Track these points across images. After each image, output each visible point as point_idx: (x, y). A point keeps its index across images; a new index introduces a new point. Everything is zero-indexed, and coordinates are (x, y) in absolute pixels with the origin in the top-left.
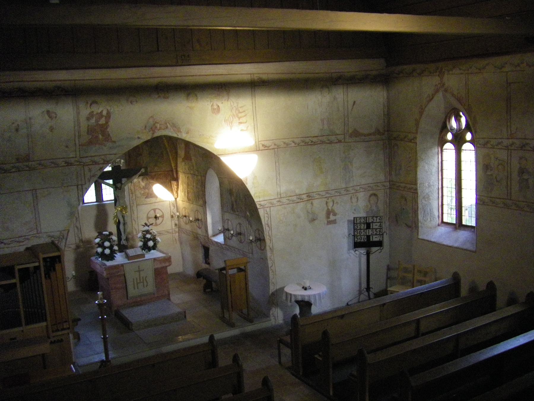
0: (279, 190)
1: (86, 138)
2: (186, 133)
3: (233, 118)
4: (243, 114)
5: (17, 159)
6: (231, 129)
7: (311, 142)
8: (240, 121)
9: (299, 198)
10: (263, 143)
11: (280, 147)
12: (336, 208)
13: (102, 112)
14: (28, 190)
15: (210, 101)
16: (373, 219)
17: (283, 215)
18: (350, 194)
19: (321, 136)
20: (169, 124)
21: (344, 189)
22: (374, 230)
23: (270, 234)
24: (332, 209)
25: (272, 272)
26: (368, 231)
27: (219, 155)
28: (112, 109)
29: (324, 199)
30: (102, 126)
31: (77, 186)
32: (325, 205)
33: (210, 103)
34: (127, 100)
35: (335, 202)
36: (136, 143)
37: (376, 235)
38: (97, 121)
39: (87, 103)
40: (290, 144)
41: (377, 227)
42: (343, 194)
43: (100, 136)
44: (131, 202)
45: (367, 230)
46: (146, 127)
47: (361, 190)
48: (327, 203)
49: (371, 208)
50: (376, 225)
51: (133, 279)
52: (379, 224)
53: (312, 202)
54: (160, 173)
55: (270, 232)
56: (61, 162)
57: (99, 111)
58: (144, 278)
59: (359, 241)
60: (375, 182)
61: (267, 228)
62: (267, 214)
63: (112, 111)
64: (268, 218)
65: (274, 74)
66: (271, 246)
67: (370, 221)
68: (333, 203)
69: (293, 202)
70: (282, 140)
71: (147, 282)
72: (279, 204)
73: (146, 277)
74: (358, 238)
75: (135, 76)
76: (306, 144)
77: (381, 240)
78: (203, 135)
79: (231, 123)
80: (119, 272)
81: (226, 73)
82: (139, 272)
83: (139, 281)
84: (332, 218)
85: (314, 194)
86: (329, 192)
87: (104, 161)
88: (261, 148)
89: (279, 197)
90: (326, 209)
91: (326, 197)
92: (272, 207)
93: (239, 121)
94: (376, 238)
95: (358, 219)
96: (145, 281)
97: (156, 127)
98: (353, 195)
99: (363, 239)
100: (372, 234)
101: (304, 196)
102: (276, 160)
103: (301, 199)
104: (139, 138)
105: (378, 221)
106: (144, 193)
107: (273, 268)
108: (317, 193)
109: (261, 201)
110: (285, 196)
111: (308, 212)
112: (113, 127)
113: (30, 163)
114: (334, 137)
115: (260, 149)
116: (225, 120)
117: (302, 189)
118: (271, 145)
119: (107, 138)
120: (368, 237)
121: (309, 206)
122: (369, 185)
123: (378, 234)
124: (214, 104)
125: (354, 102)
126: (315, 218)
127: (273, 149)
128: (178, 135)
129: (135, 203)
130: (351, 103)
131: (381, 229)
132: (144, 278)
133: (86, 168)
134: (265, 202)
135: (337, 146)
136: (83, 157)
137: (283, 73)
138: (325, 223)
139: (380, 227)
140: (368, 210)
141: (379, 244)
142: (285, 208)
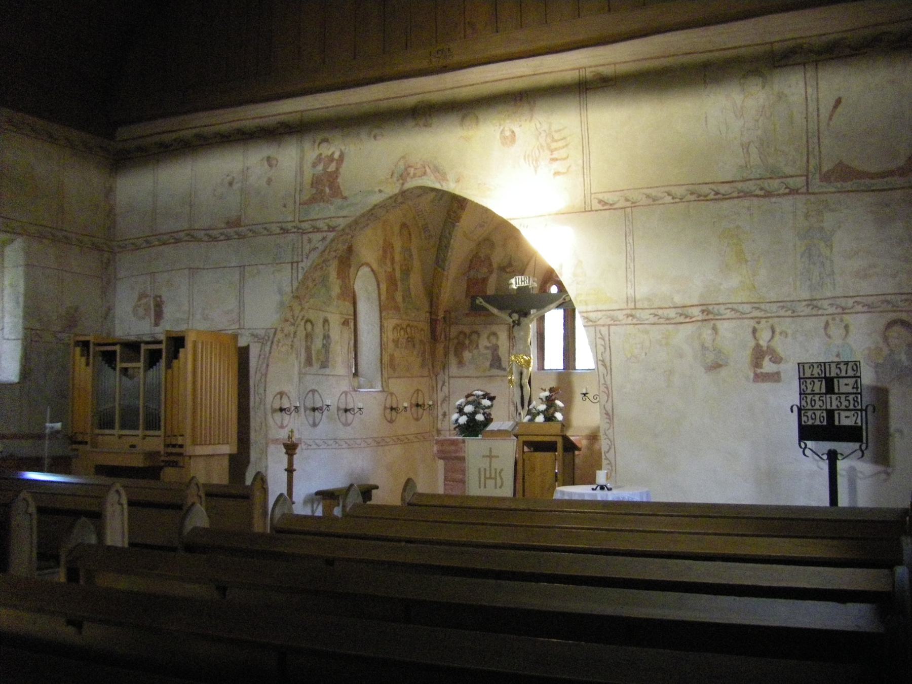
1: (306, 196)
2: (456, 182)
3: (539, 152)
4: (560, 144)
5: (228, 223)
7: (715, 195)
8: (554, 156)
9: (681, 315)
10: (600, 196)
11: (638, 204)
12: (779, 345)
13: (333, 153)
14: (292, 285)
15: (498, 124)
16: (840, 368)
17: (638, 346)
20: (430, 168)
22: (843, 397)
23: (609, 383)
24: (768, 347)
25: (608, 464)
26: (828, 400)
27: (510, 219)
28: (347, 149)
29: (746, 321)
31: (292, 263)
33: (500, 128)
34: (369, 135)
35: (778, 331)
36: (376, 199)
38: (325, 169)
39: (314, 142)
41: (849, 389)
43: (327, 190)
45: (828, 396)
47: (859, 308)
48: (754, 331)
51: (480, 470)
52: (851, 381)
53: (714, 325)
56: (275, 228)
57: (330, 153)
58: (498, 472)
59: (810, 422)
64: (605, 349)
65: (628, 62)
67: (833, 375)
68: (773, 332)
69: (668, 322)
71: (501, 479)
72: (630, 320)
73: (502, 470)
74: (807, 416)
75: (381, 96)
76: (702, 198)
77: (860, 424)
78: (485, 184)
81: (531, 73)
82: (493, 457)
83: (488, 475)
84: (768, 366)
86: (763, 306)
87: (329, 227)
88: (596, 205)
89: (632, 305)
90: (752, 344)
94: (846, 417)
95: (806, 366)
96: (498, 478)
97: (408, 174)
98: (834, 319)
100: (837, 406)
101: (696, 311)
102: (628, 230)
103: (686, 317)
104: (380, 191)
105: (850, 373)
107: (611, 455)
108: (730, 306)
109: (591, 312)
111: (704, 347)
112: (348, 176)
113: (240, 229)
114: (778, 181)
115: (587, 209)
116: (525, 156)
118: (619, 200)
119: (336, 192)
120: (830, 414)
121: (707, 333)
122: (889, 298)
123: (851, 407)
124: (506, 129)
125: (838, 102)
126: (721, 363)
127: (621, 208)
128: (442, 186)
132: (498, 472)
133: (305, 237)
134: (599, 315)
135: (787, 203)
138: (747, 378)
139: (855, 391)
140: (880, 361)
142: (647, 332)
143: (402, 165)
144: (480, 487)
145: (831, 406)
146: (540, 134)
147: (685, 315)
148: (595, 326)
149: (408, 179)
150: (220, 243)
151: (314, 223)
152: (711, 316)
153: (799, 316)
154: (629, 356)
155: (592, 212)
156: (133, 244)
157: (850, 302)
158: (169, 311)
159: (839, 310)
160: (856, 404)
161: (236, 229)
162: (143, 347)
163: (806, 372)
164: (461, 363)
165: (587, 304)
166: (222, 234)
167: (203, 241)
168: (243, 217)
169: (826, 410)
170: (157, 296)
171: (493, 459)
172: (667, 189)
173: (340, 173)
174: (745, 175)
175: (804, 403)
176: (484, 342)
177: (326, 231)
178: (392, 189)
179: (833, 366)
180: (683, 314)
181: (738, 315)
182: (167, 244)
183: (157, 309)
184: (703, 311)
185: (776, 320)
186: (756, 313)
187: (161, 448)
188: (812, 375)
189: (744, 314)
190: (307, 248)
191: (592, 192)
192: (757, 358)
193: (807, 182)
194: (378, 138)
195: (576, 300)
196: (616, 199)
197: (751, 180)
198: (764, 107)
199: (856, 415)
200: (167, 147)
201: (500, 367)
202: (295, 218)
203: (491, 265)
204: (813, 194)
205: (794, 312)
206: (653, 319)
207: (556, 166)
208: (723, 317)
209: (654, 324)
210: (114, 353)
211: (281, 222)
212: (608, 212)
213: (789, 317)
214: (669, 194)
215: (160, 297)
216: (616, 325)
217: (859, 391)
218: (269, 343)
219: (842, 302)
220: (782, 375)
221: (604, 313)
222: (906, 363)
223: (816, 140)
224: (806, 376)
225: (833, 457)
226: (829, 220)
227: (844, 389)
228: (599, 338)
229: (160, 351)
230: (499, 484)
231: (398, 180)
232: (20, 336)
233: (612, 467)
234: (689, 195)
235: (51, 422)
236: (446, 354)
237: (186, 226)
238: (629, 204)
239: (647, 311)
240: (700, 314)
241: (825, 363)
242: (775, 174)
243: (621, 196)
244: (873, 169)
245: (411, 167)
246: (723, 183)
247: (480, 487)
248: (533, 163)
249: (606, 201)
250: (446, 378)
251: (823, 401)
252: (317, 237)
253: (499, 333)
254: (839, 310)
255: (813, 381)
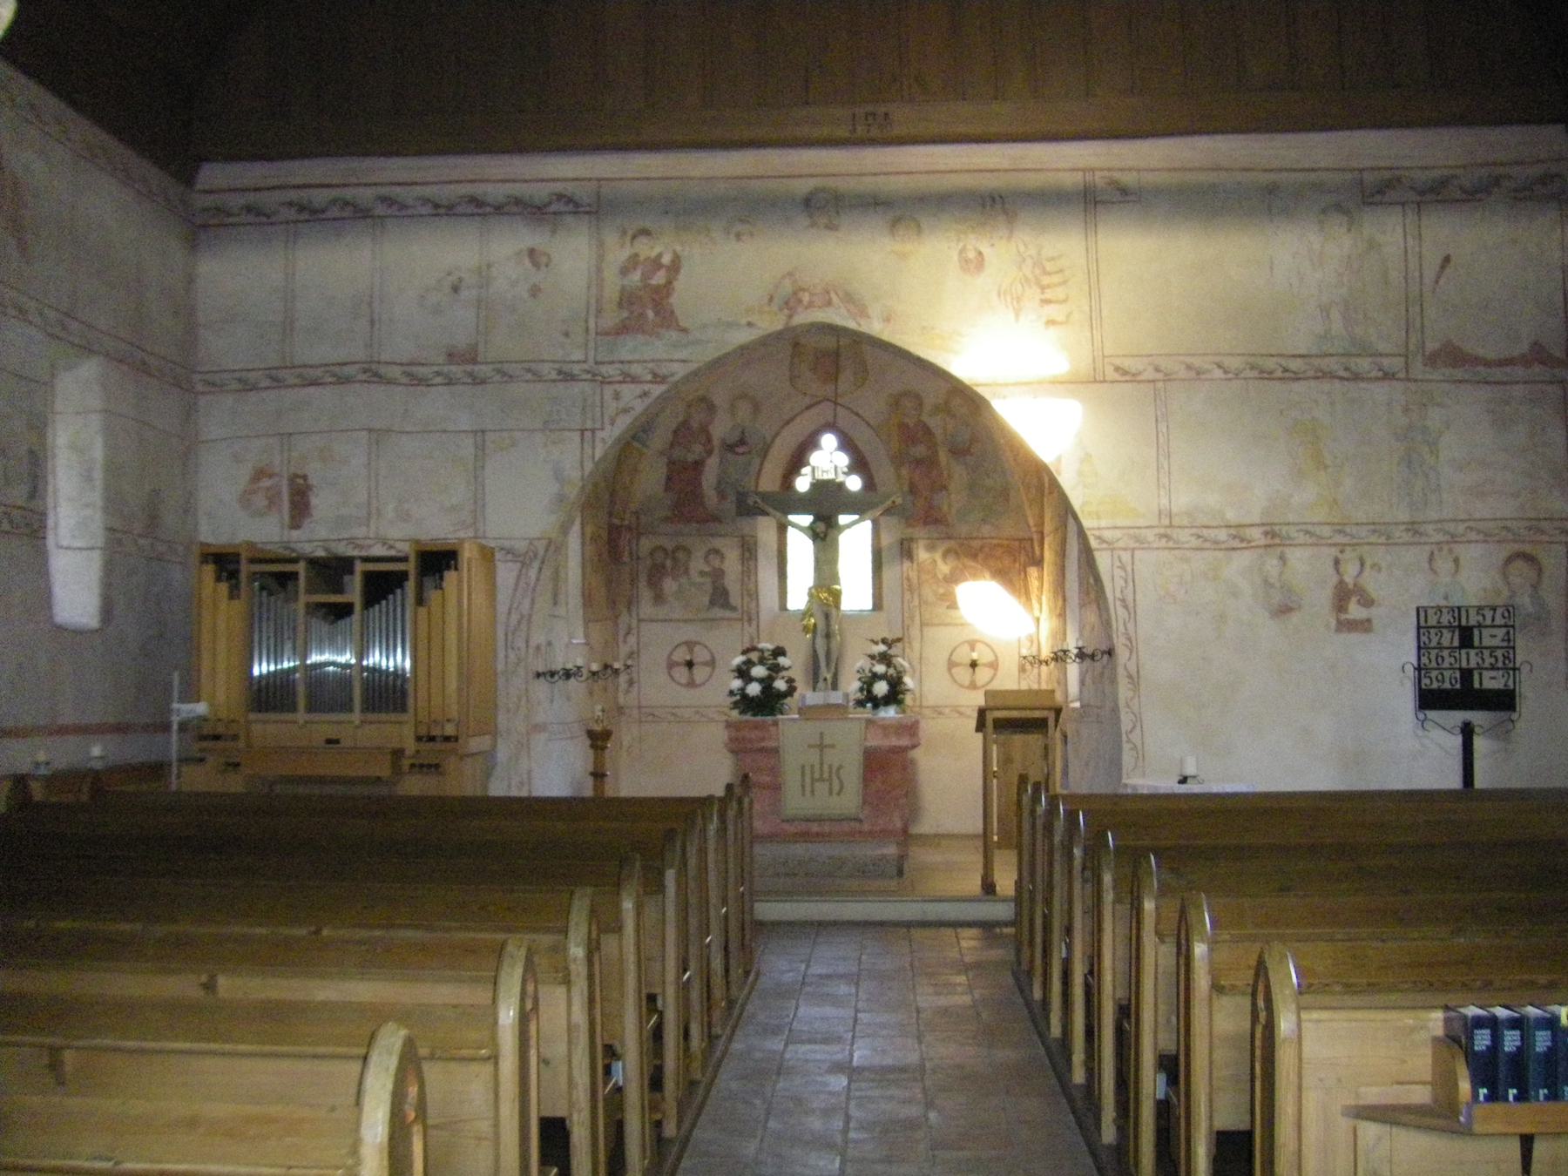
0: (1164, 501)
1: (611, 318)
2: (884, 321)
3: (1023, 286)
4: (1056, 279)
6: (1017, 315)
7: (1283, 372)
9: (1235, 537)
10: (1118, 362)
12: (1371, 583)
13: (660, 255)
16: (1484, 616)
18: (1425, 543)
19: (1317, 356)
20: (836, 294)
21: (1404, 527)
22: (1486, 653)
23: (1131, 631)
24: (1355, 585)
25: (1132, 749)
26: (1464, 656)
27: (977, 385)
29: (1326, 550)
30: (657, 289)
31: (582, 431)
32: (1331, 570)
34: (727, 231)
35: (1368, 563)
36: (743, 337)
37: (1493, 668)
38: (646, 277)
40: (1208, 371)
42: (1397, 541)
43: (650, 314)
44: (906, 615)
45: (1463, 652)
46: (771, 299)
47: (1473, 536)
48: (1337, 562)
49: (1511, 597)
50: (1493, 636)
51: (803, 767)
54: (995, 542)
55: (1130, 626)
56: (547, 370)
57: (654, 254)
59: (1435, 685)
60: (1532, 514)
61: (1121, 611)
62: (1123, 568)
63: (686, 253)
64: (1126, 582)
66: (1132, 668)
67: (1472, 622)
68: (1362, 565)
70: (1181, 358)
71: (841, 782)
73: (840, 767)
76: (1266, 375)
77: (1512, 687)
79: (1018, 302)
80: (763, 739)
83: (817, 775)
84: (1355, 611)
85: (1293, 531)
87: (655, 375)
88: (1111, 374)
89: (1166, 522)
90: (1335, 580)
91: (1335, 545)
92: (1139, 549)
93: (1043, 297)
95: (1430, 612)
96: (834, 777)
97: (800, 301)
99: (1447, 680)
100: (1478, 664)
101: (1256, 534)
102: (1159, 413)
103: (1242, 540)
104: (750, 324)
105: (1499, 621)
106: (943, 595)
108: (1304, 527)
109: (1103, 528)
110: (1185, 522)
111: (1267, 583)
112: (683, 297)
113: (476, 368)
117: (1252, 507)
118: (1145, 370)
119: (667, 318)
120: (1467, 675)
121: (1272, 565)
122: (1509, 524)
123: (1500, 665)
124: (969, 247)
127: (1149, 381)
128: (860, 325)
129: (917, 619)
130: (1432, 260)
131: (1511, 652)
132: (834, 771)
133: (609, 391)
134: (1118, 533)
135: (1380, 391)
136: (603, 363)
137: (1201, 169)
139: (1505, 644)
141: (1504, 701)
142: (1187, 560)
143: (788, 286)
144: (803, 795)
145: (1468, 663)
146: (1024, 260)
147: (1239, 537)
148: (1113, 550)
149: (800, 309)
150: (434, 389)
151: (626, 367)
152: (1277, 541)
153: (1396, 544)
154: (1162, 593)
155: (1105, 385)
156: (240, 380)
157: (1461, 528)
158: (322, 502)
159: (1448, 538)
160: (1507, 662)
161: (469, 368)
162: (359, 567)
163: (1429, 617)
164: (659, 598)
165: (1099, 518)
166: (438, 374)
167: (400, 384)
168: (481, 348)
169: (1460, 669)
170: (297, 476)
171: (826, 750)
172: (1218, 359)
173: (673, 289)
174: (1324, 348)
175: (1424, 660)
176: (697, 564)
177: (647, 382)
178: (771, 323)
179: (1472, 612)
180: (1238, 537)
181: (1314, 540)
182: (321, 384)
183: (297, 498)
184: (1266, 534)
185: (1366, 548)
186: (1339, 539)
187: (410, 746)
188: (1439, 622)
189: (1322, 538)
190: (612, 407)
191: (1106, 354)
192: (1340, 601)
193: (1406, 363)
194: (744, 238)
195: (1083, 512)
196: (1141, 368)
197: (1332, 355)
198: (1349, 257)
199: (1506, 675)
200: (314, 212)
201: (726, 605)
202: (586, 354)
203: (709, 440)
204: (1416, 381)
205: (1388, 538)
206: (1195, 542)
207: (1052, 311)
208: (1296, 542)
209: (1197, 549)
210: (293, 576)
211: (558, 362)
212: (1130, 385)
213: (1382, 544)
214: (1219, 366)
215: (305, 477)
216: (1143, 549)
217: (1512, 644)
218: (536, 565)
219: (1451, 527)
220: (1375, 622)
221: (1125, 531)
222: (1531, 609)
223: (1417, 309)
224: (1429, 624)
225: (1467, 732)
226: (1435, 417)
227: (1487, 642)
228: (1118, 567)
229: (404, 576)
230: (836, 788)
231: (781, 309)
232: (100, 542)
233: (1137, 753)
234: (1248, 371)
235: (182, 700)
236: (634, 581)
237: (360, 354)
238: (1160, 376)
239: (1186, 530)
240: (1263, 537)
241: (1459, 608)
242: (1364, 349)
243: (1149, 364)
244: (1491, 355)
245: (803, 290)
246: (1294, 356)
247: (803, 795)
248: (1012, 303)
249: (1127, 368)
250: (634, 623)
251: (1455, 657)
252: (629, 392)
253: (724, 550)
254: (1448, 538)
255: (1441, 632)
